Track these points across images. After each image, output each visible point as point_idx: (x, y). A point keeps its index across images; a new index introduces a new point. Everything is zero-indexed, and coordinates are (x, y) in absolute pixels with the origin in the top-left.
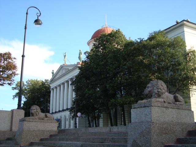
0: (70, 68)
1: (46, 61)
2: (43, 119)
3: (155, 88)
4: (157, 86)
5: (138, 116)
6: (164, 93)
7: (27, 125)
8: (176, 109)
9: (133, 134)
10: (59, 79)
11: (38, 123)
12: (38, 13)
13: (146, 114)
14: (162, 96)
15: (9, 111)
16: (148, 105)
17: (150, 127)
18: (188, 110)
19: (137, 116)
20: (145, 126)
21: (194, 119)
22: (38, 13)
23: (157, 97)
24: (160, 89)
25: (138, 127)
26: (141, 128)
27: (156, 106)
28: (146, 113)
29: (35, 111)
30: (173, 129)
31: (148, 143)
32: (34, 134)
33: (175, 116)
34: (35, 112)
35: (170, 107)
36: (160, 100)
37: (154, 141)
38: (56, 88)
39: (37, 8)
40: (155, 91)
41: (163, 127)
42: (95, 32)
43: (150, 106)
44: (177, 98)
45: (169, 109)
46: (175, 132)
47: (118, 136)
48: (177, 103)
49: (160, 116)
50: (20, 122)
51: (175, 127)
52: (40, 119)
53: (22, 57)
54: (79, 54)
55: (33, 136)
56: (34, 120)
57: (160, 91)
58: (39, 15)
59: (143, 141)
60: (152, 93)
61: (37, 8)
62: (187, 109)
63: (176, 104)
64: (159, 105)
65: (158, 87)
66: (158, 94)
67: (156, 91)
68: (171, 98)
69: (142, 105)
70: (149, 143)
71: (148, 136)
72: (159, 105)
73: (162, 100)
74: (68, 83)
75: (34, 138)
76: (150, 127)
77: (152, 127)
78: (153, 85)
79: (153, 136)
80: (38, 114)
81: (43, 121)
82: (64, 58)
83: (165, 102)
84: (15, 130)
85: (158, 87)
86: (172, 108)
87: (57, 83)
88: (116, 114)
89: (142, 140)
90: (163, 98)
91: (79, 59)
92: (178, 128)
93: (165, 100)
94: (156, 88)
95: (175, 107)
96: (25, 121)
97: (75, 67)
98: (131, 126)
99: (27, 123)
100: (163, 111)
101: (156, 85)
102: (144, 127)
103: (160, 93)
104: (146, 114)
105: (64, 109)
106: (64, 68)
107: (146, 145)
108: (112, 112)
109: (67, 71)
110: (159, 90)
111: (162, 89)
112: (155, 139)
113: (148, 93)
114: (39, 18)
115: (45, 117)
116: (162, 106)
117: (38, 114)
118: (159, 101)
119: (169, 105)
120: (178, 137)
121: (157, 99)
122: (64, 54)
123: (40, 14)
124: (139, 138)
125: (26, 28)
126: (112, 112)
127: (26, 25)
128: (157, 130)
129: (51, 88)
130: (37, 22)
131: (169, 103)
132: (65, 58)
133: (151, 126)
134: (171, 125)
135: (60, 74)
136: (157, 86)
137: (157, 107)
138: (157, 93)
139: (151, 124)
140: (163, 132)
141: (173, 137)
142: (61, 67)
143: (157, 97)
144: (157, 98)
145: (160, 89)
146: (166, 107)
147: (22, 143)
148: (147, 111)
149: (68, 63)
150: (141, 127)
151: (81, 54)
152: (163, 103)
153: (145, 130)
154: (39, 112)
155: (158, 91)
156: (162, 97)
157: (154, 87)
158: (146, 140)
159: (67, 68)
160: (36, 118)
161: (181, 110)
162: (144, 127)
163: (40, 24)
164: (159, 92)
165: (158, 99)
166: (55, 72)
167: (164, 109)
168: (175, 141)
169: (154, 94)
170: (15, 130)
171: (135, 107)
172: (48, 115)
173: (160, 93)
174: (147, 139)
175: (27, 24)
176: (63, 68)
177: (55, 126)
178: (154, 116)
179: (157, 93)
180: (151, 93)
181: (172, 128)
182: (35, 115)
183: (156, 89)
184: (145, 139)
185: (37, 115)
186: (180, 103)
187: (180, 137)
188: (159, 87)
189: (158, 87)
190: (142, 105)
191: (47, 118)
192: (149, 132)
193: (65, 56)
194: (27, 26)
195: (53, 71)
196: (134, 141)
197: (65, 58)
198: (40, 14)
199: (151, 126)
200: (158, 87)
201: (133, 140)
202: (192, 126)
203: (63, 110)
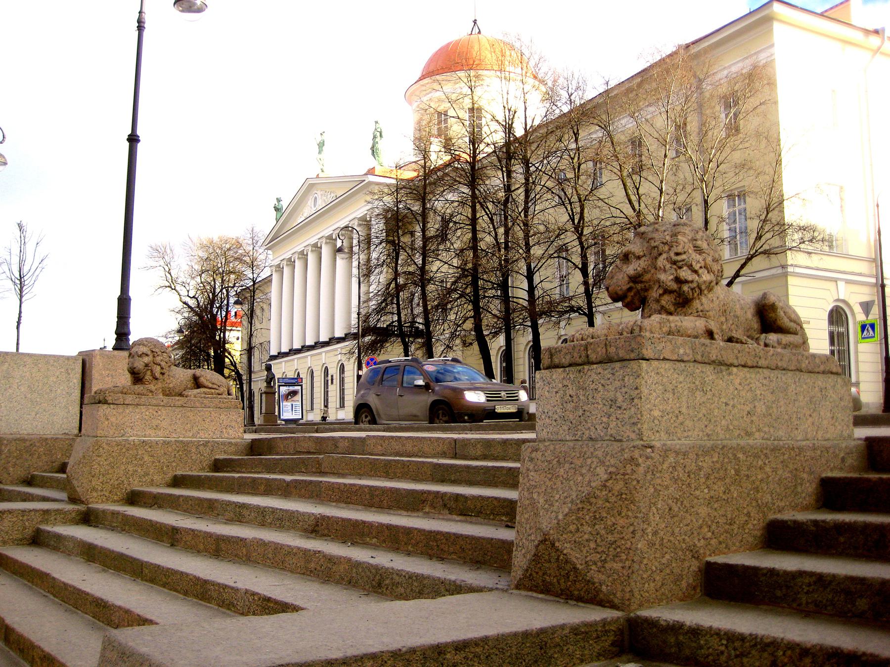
1: (765, 294)
2: (181, 395)
3: (661, 261)
4: (675, 250)
5: (570, 406)
6: (710, 289)
7: (113, 419)
8: (766, 372)
9: (542, 501)
11: (164, 411)
13: (614, 401)
14: (696, 304)
15: (68, 358)
16: (622, 354)
17: (633, 471)
18: (823, 373)
19: (564, 410)
20: (602, 463)
23: (672, 309)
24: (690, 267)
25: (567, 466)
26: (582, 475)
27: (664, 359)
28: (611, 395)
29: (146, 360)
30: (747, 476)
31: (617, 556)
32: (146, 458)
33: (761, 408)
34: (147, 365)
35: (736, 362)
36: (689, 322)
37: (651, 544)
40: (663, 277)
41: (700, 469)
42: (436, 53)
43: (633, 356)
44: (772, 315)
45: (735, 370)
46: (757, 490)
48: (773, 337)
49: (684, 410)
51: (760, 463)
54: (375, 137)
55: (142, 466)
56: (144, 399)
57: (690, 279)
59: (592, 545)
60: (646, 290)
62: (822, 368)
63: (766, 345)
64: (681, 351)
65: (677, 254)
66: (679, 293)
67: (666, 278)
68: (739, 313)
69: (594, 351)
70: (624, 557)
71: (621, 522)
72: (681, 351)
73: (700, 324)
76: (633, 471)
77: (641, 470)
78: (653, 244)
79: (646, 520)
80: (163, 374)
81: (181, 401)
82: (320, 153)
83: (710, 334)
85: (677, 254)
86: (750, 363)
88: (508, 356)
89: (586, 536)
90: (702, 314)
92: (775, 470)
93: (713, 326)
94: (669, 260)
95: (762, 362)
96: (106, 402)
97: (359, 187)
98: (531, 460)
100: (703, 383)
101: (666, 248)
102: (601, 471)
103: (685, 288)
104: (614, 401)
105: (308, 344)
107: (608, 566)
108: (497, 344)
110: (685, 274)
111: (697, 267)
112: (655, 533)
113: (625, 288)
115: (190, 385)
116: (699, 358)
117: (163, 374)
118: (679, 332)
119: (730, 353)
120: (772, 516)
121: (671, 318)
122: (319, 139)
124: (572, 528)
126: (497, 344)
128: (667, 487)
131: (730, 340)
133: (638, 465)
134: (740, 455)
135: (308, 210)
136: (675, 250)
137: (668, 365)
138: (674, 286)
139: (636, 454)
140: (697, 493)
141: (748, 514)
143: (672, 309)
144: (671, 314)
145: (690, 267)
146: (720, 364)
148: (618, 384)
150: (584, 471)
152: (703, 340)
153: (605, 486)
154: (163, 364)
155: (678, 280)
156: (700, 308)
157: (656, 258)
158: (610, 538)
160: (151, 392)
161: (790, 374)
162: (601, 471)
163: (200, 10)
164: (686, 282)
165: (675, 321)
167: (708, 369)
168: (759, 533)
169: (654, 294)
171: (556, 361)
172: (202, 380)
173: (685, 288)
174: (611, 532)
175: (145, 9)
177: (233, 424)
178: (656, 413)
179: (674, 286)
180: (639, 286)
181: (744, 471)
182: (148, 377)
183: (668, 266)
184: (603, 532)
186: (786, 339)
187: (779, 516)
188: (684, 257)
189: (679, 258)
190: (594, 351)
191: (202, 390)
192: (626, 499)
193: (321, 145)
194: (147, 18)
195: (279, 200)
196: (545, 540)
199: (638, 465)
200: (679, 258)
201: (539, 538)
202: (842, 455)
203: (318, 345)
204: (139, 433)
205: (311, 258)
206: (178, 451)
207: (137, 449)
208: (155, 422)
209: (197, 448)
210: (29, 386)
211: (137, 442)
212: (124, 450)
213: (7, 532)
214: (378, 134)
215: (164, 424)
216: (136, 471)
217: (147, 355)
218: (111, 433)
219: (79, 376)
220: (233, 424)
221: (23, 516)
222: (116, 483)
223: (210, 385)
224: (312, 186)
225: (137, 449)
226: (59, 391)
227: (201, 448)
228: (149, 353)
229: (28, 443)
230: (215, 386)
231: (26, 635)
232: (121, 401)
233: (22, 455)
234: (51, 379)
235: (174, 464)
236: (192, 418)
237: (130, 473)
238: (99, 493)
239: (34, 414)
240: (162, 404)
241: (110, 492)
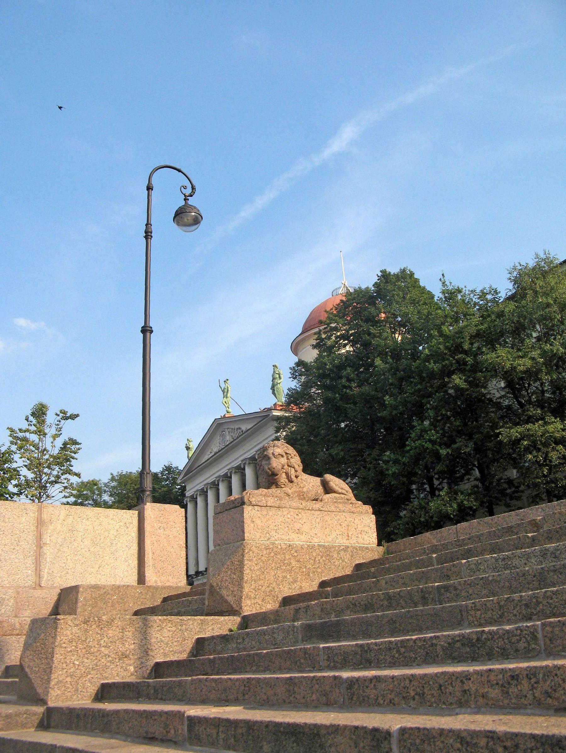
0: (244, 427)
7: (258, 522)
10: (211, 464)
12: (185, 188)
21: (108, 684)
22: (185, 188)
32: (294, 563)
38: (204, 493)
39: (179, 171)
47: (239, 650)
50: (221, 516)
52: (302, 496)
53: (152, 323)
54: (274, 379)
55: (290, 571)
58: (188, 191)
61: (179, 171)
74: (218, 490)
75: (295, 581)
80: (297, 477)
81: (318, 505)
84: (156, 582)
87: (204, 479)
91: (274, 393)
99: (259, 514)
105: (200, 570)
106: (226, 426)
109: (235, 435)
114: (191, 201)
115: (321, 490)
117: (297, 477)
123: (193, 188)
125: (148, 235)
127: (148, 224)
129: (188, 494)
130: (186, 217)
132: (226, 396)
135: (215, 447)
142: (219, 426)
147: (248, 602)
149: (235, 411)
151: (280, 378)
159: (237, 427)
160: (288, 495)
166: (194, 445)
170: (156, 582)
176: (221, 429)
177: (366, 529)
182: (283, 478)
185: (291, 482)
193: (225, 392)
194: (153, 228)
197: (226, 396)
198: (193, 188)
204: (283, 537)
205: (235, 481)
206: (322, 557)
207: (284, 554)
208: (297, 526)
209: (338, 553)
210: (92, 540)
211: (284, 547)
212: (272, 554)
213: (167, 644)
214: (278, 376)
215: (305, 528)
216: (286, 577)
217: (282, 456)
218: (258, 537)
219: (135, 529)
220: (366, 529)
221: (181, 625)
222: (268, 590)
223: (340, 491)
224: (220, 425)
225: (284, 554)
226: (119, 545)
227: (342, 553)
228: (284, 454)
229: (102, 591)
230: (344, 491)
231: (304, 713)
232: (263, 503)
233: (97, 603)
234: (112, 532)
235: (319, 570)
236: (330, 522)
237: (280, 579)
238: (253, 601)
239: (97, 566)
240: (301, 507)
241: (263, 600)
